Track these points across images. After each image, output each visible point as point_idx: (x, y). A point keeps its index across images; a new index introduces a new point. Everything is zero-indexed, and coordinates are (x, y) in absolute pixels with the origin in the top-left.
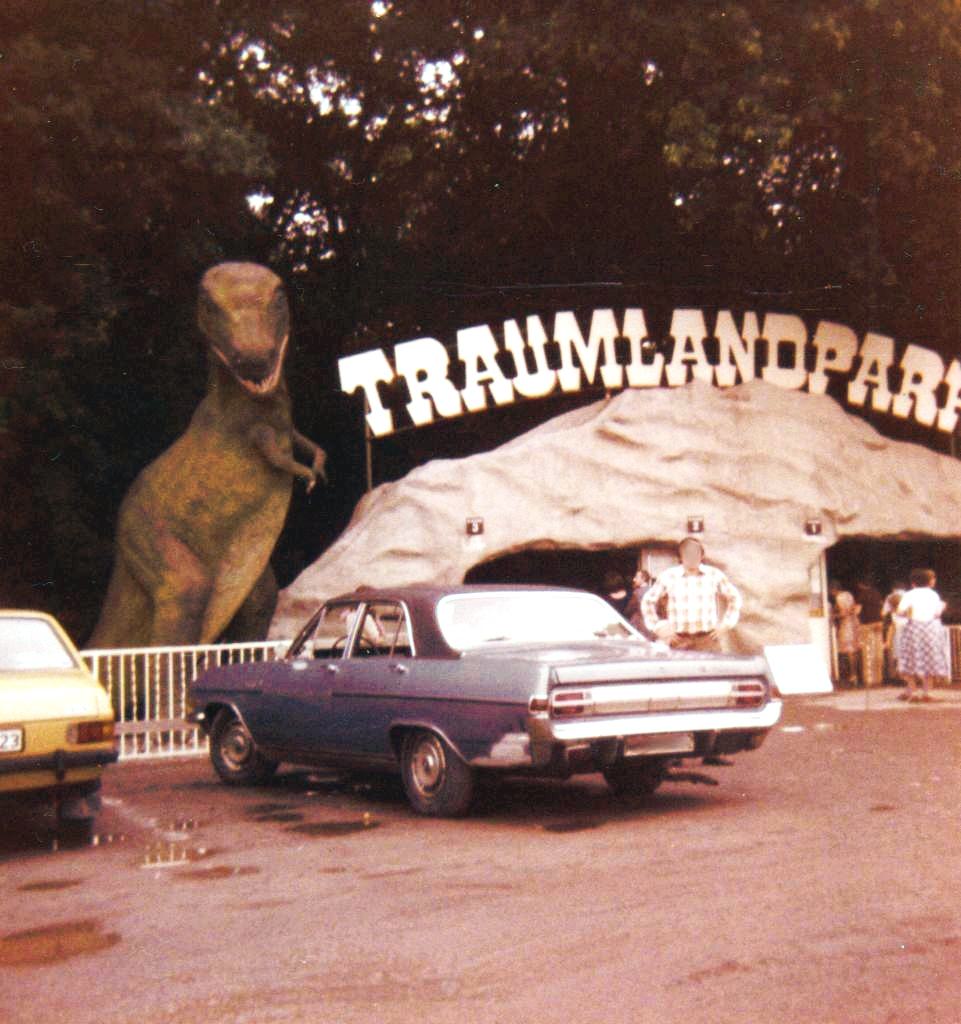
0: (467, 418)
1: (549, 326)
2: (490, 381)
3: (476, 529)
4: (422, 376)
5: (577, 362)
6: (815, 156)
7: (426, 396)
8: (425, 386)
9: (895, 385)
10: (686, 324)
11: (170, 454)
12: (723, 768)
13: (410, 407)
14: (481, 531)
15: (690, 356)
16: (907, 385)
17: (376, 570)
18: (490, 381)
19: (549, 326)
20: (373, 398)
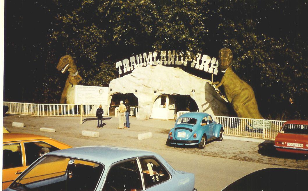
0: (198, 70)
1: (142, 55)
2: (196, 64)
3: (193, 91)
4: (205, 62)
5: (146, 61)
6: (205, 31)
7: (204, 65)
8: (204, 64)
9: (200, 63)
10: (163, 54)
11: (235, 78)
12: (48, 147)
13: (124, 70)
14: (156, 93)
15: (163, 59)
16: (203, 63)
17: (100, 107)
18: (196, 64)
19: (142, 55)
20: (120, 68)
